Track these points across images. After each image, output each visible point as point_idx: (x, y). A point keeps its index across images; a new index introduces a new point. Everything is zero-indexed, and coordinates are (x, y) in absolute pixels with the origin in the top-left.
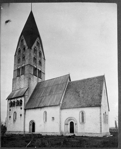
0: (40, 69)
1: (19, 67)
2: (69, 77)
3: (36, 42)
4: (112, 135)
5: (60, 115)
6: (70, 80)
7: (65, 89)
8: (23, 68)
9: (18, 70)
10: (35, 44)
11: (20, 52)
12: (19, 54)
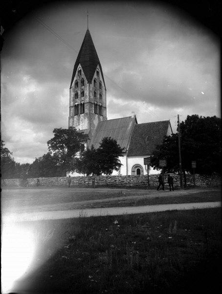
0: (101, 104)
1: (76, 104)
2: (136, 119)
3: (96, 72)
4: (102, 148)
5: (127, 162)
6: (137, 123)
7: (112, 199)
8: (83, 105)
9: (76, 107)
10: (95, 76)
11: (78, 85)
12: (75, 87)
